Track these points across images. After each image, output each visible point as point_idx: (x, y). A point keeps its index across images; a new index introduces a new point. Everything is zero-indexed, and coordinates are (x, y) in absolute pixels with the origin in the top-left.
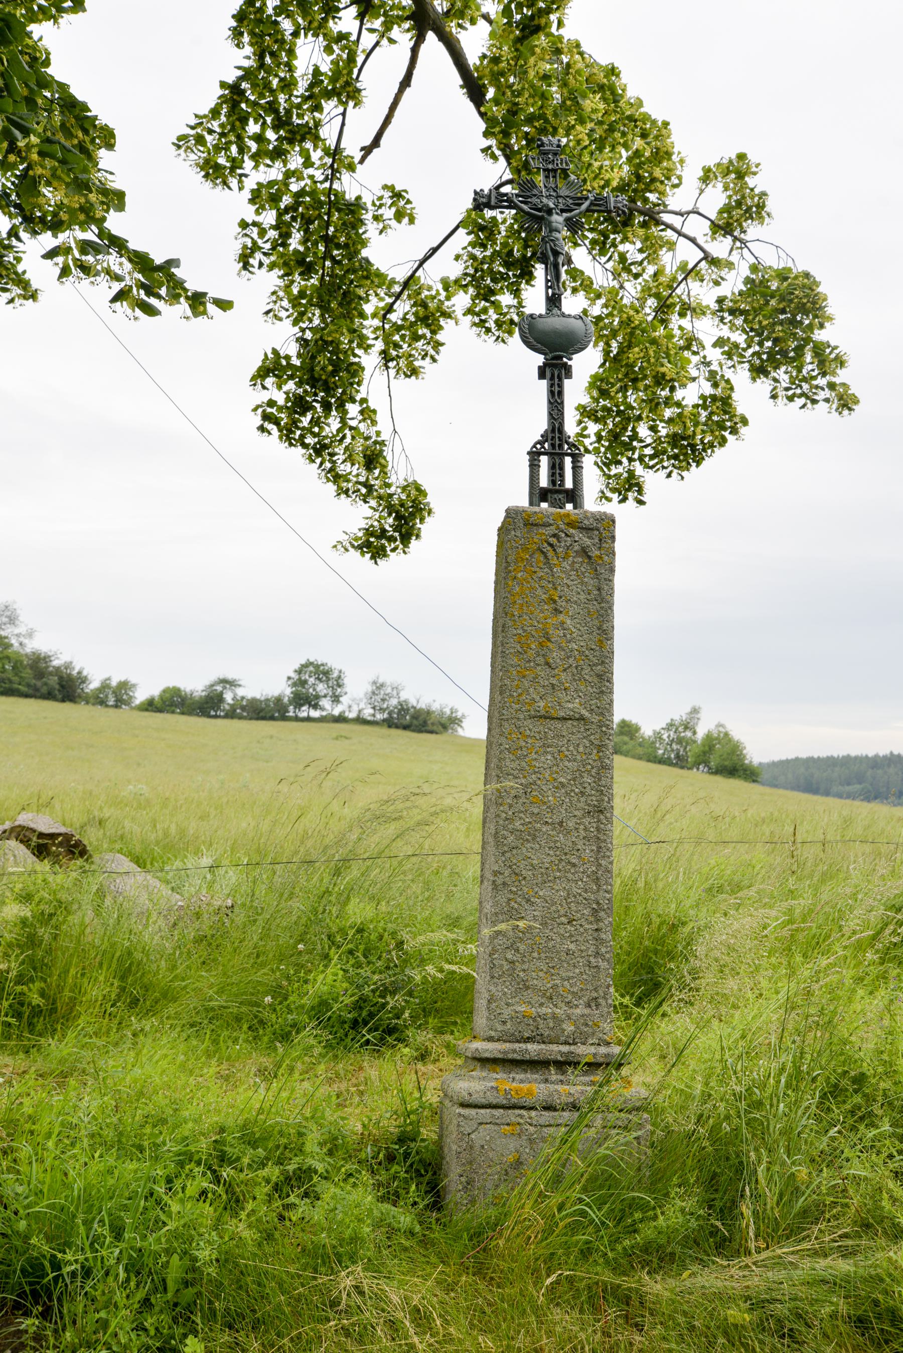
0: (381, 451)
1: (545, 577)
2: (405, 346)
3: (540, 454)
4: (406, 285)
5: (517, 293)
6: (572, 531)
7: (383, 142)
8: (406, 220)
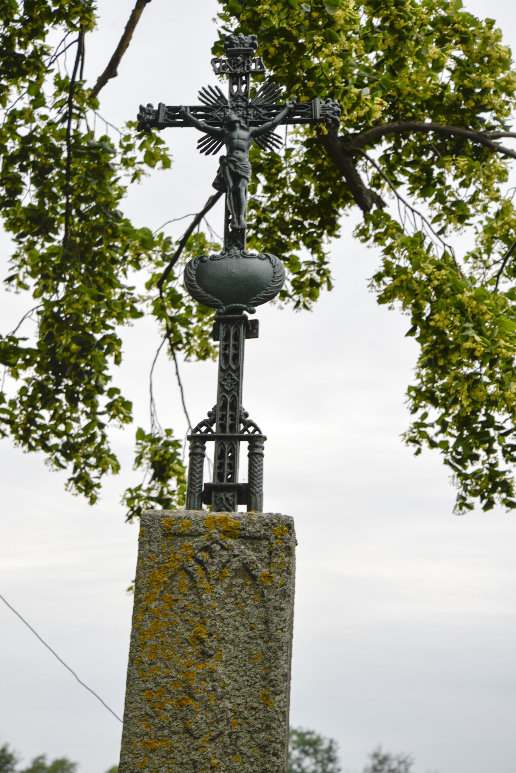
0: (177, 454)
1: (191, 607)
2: (194, 320)
3: (204, 438)
4: (183, 243)
5: (314, 245)
6: (230, 541)
7: (120, 69)
8: (159, 164)
